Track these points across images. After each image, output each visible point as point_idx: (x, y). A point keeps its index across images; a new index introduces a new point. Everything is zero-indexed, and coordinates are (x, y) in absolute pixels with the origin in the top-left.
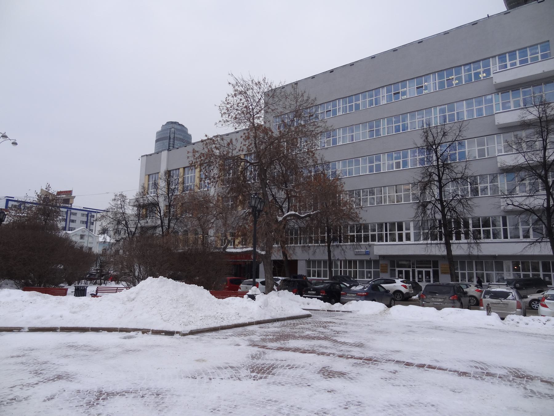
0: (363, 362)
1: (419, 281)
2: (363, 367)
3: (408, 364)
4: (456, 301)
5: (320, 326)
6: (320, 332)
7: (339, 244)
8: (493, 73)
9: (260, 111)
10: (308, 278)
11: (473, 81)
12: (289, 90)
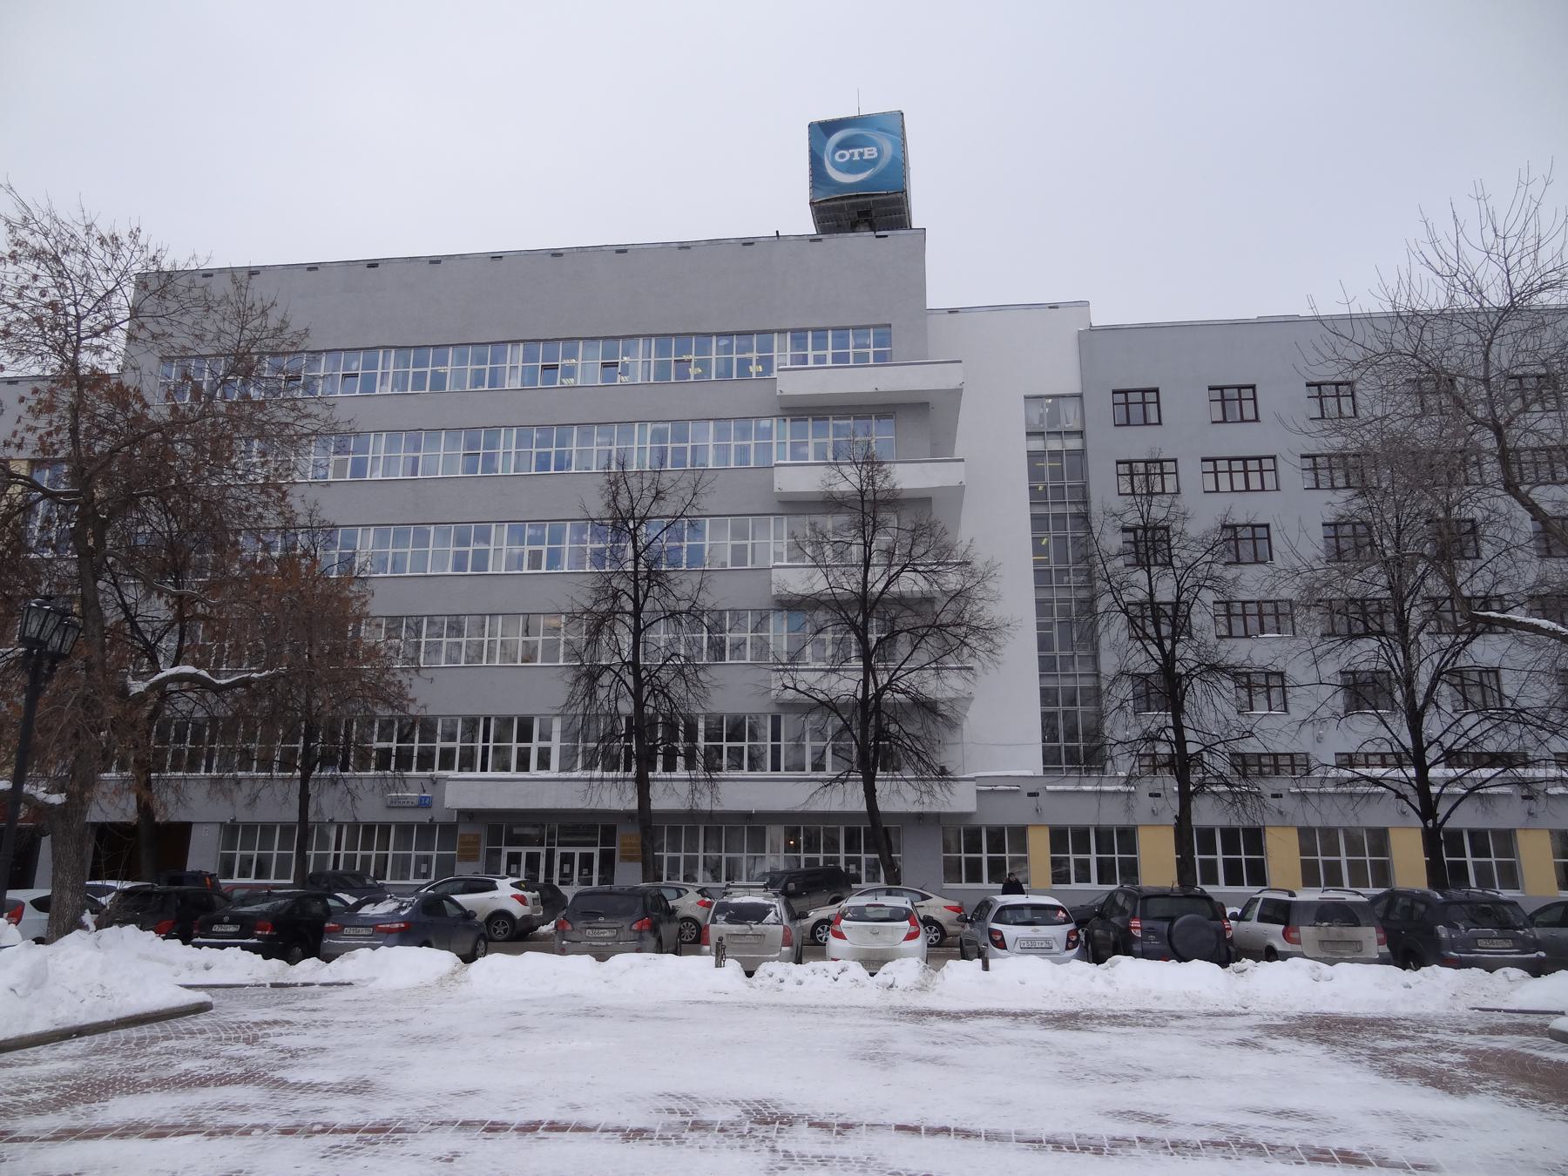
0: (359, 1140)
1: (561, 883)
2: (357, 1156)
3: (494, 1128)
4: (646, 935)
5: (237, 1040)
6: (233, 1059)
7: (338, 773)
8: (779, 370)
9: (107, 329)
10: (221, 881)
11: (735, 377)
12: (219, 288)
